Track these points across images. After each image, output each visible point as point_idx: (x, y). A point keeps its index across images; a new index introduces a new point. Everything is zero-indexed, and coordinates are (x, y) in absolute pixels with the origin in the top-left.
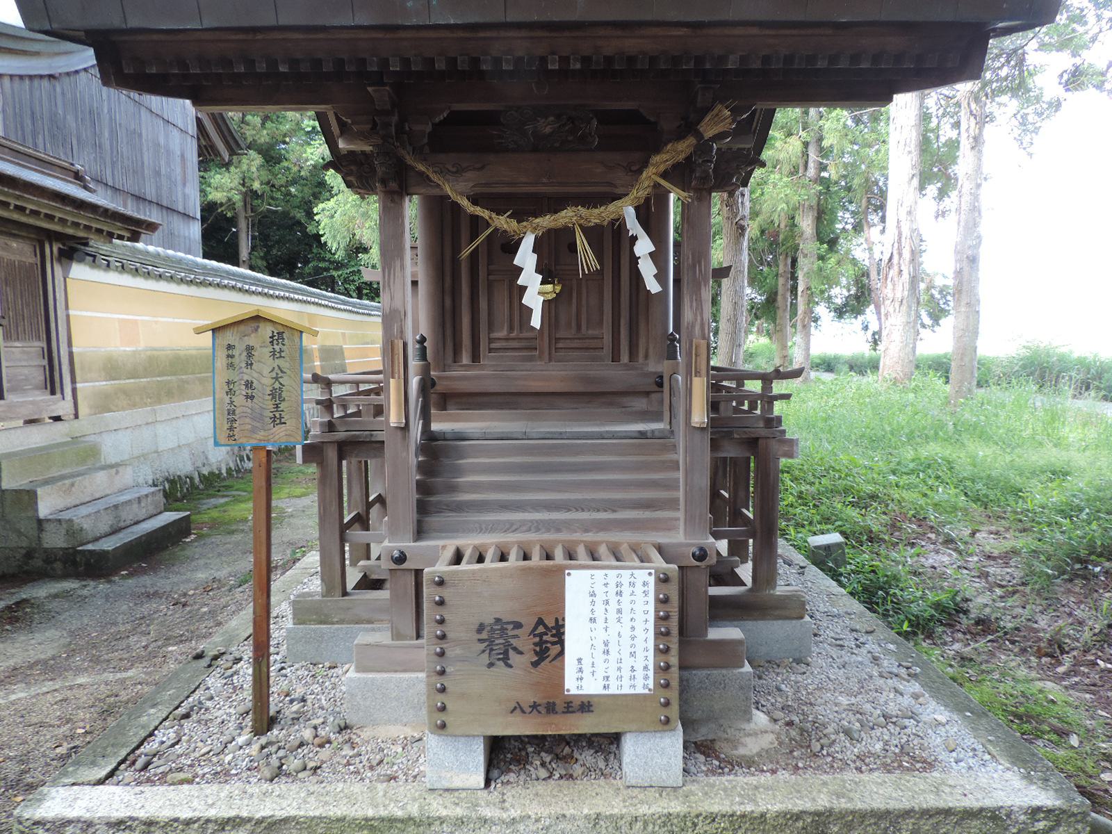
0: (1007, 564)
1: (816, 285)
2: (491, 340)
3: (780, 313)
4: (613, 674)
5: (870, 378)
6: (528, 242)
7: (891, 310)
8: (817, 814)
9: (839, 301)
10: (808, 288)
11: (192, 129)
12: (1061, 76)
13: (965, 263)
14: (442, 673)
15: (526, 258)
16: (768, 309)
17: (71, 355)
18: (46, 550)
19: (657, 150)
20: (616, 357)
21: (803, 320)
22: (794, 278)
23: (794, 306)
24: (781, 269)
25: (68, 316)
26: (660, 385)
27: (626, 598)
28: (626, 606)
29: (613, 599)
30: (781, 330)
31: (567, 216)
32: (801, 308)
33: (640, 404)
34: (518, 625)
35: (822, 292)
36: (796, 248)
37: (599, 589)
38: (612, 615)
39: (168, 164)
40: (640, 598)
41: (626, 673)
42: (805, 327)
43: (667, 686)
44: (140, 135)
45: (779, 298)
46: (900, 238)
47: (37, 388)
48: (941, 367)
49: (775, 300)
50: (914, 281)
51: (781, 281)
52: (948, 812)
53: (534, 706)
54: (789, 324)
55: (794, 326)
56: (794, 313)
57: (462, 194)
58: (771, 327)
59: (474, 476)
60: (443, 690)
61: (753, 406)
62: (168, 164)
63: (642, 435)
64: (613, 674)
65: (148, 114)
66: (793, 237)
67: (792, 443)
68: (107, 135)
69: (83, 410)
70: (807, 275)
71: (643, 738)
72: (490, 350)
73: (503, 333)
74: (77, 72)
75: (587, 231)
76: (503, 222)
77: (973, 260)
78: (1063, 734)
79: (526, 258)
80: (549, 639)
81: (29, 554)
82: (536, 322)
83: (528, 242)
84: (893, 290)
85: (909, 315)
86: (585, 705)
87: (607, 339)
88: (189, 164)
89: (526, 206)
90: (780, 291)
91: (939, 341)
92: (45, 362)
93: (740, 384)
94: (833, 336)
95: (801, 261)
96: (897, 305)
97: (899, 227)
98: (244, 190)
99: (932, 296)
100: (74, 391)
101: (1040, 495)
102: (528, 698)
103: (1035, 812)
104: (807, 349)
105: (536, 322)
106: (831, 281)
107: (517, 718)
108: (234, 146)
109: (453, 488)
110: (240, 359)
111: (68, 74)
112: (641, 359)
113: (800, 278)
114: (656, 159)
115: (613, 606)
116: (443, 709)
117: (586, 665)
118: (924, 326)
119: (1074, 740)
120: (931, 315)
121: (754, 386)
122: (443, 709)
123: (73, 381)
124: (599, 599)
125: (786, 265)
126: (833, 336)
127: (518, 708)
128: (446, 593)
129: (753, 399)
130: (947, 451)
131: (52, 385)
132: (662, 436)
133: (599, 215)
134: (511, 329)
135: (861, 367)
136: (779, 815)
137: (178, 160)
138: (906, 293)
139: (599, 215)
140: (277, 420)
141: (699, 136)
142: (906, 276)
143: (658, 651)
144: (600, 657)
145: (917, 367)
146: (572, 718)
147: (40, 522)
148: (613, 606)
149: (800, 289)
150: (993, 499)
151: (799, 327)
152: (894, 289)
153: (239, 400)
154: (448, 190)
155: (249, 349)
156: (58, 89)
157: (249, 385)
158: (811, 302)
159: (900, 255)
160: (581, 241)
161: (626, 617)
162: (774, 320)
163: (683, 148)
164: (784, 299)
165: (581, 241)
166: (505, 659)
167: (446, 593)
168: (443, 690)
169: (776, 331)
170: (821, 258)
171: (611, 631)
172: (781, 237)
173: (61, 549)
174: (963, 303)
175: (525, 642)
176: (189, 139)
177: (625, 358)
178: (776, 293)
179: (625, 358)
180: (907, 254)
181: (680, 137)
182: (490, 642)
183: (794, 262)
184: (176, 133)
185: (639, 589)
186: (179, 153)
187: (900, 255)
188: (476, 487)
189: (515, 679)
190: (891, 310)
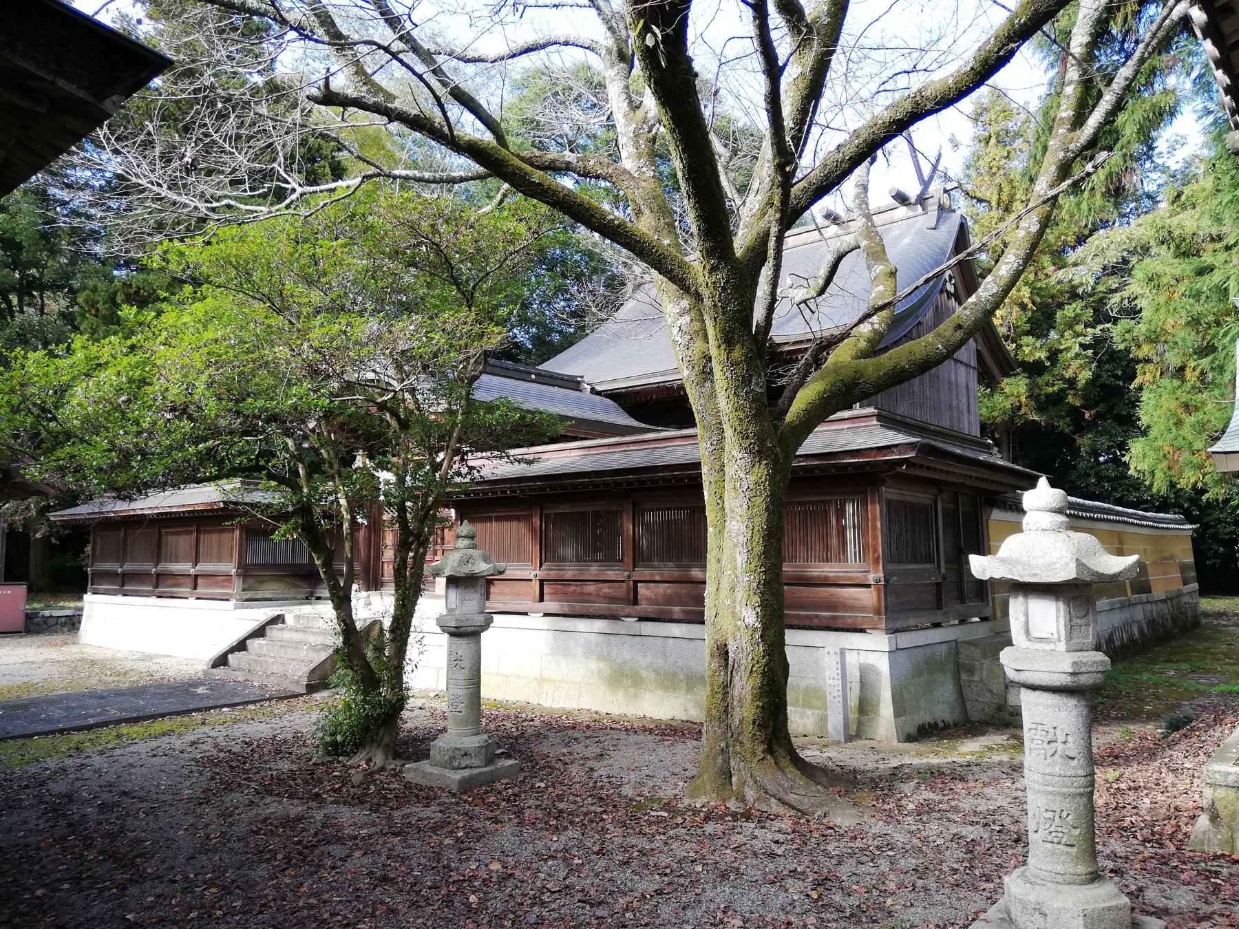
184: (962, 369)
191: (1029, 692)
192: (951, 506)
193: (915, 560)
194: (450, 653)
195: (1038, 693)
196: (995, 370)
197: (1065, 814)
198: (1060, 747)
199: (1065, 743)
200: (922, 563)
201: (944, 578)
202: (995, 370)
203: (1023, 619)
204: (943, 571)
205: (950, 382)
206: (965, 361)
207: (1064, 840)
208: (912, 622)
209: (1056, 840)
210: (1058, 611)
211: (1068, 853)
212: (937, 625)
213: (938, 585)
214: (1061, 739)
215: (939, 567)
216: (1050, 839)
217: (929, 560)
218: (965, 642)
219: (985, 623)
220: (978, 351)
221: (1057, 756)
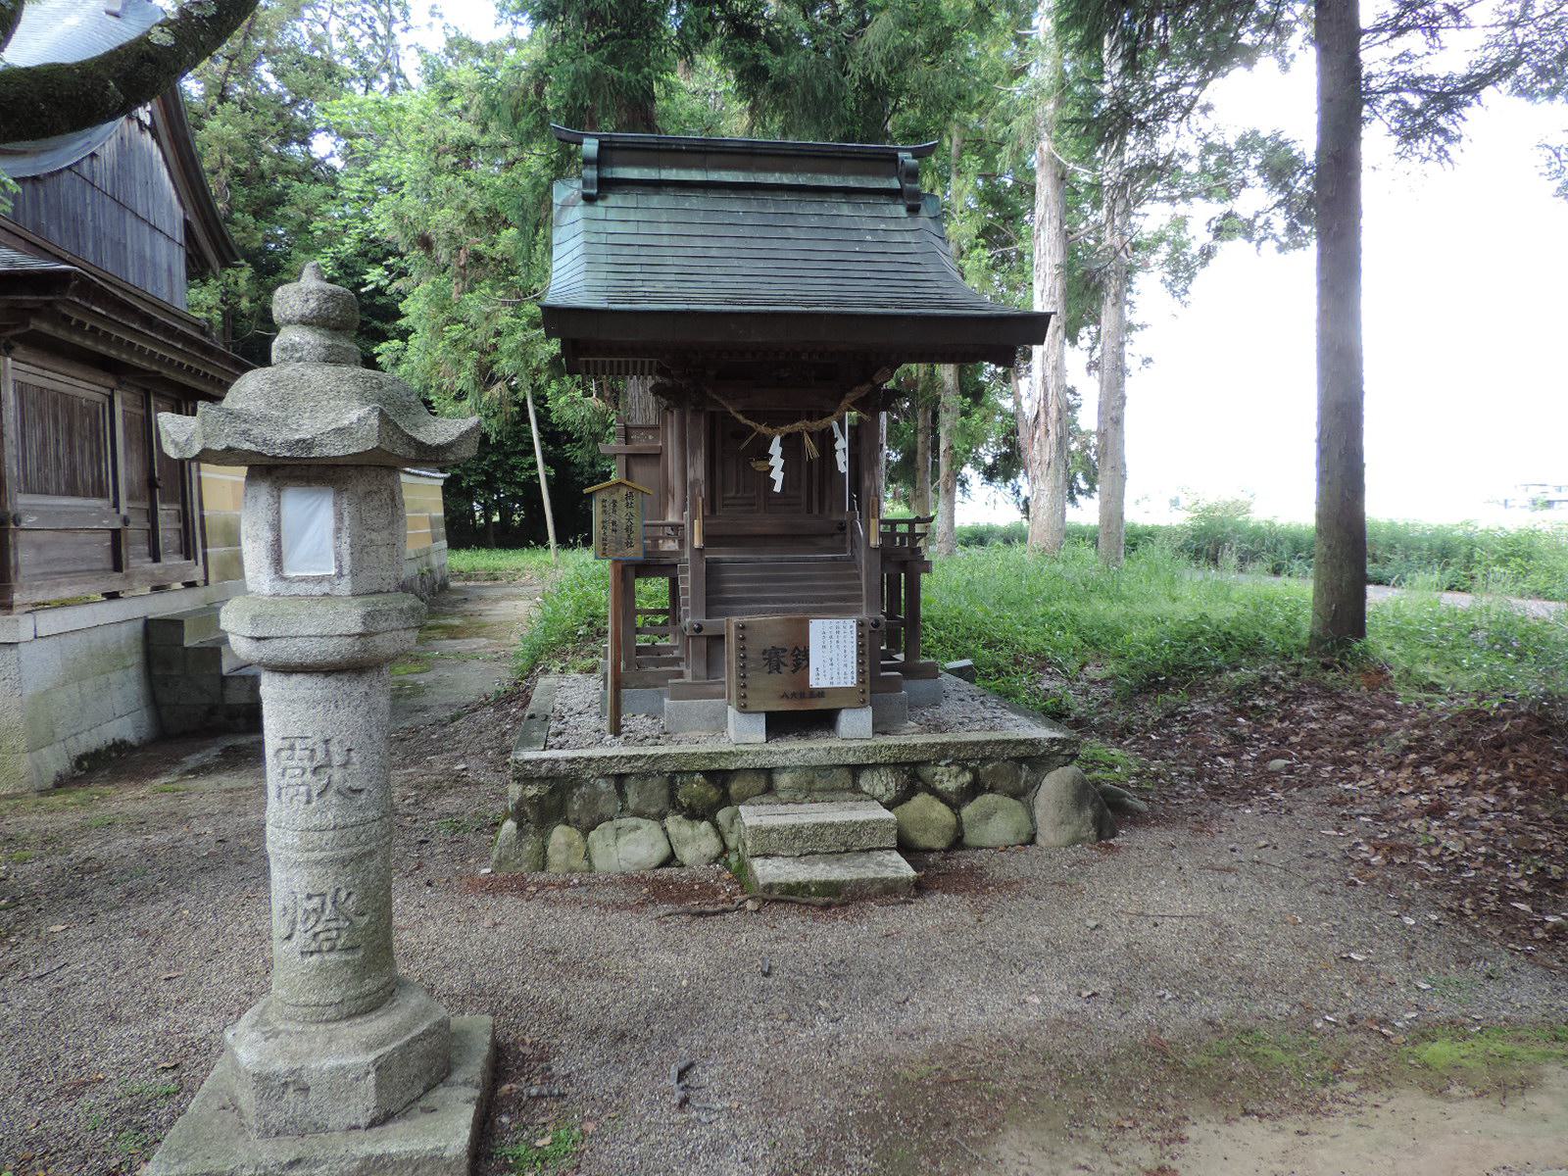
0: (1104, 686)
1: (960, 445)
2: (724, 499)
3: (920, 475)
4: (835, 676)
5: (1018, 548)
6: (777, 440)
7: (1039, 473)
8: (944, 744)
9: (989, 460)
10: (951, 448)
11: (179, 236)
12: (1209, 223)
13: (1109, 425)
14: (744, 677)
15: (776, 449)
16: (907, 471)
17: (202, 517)
18: (229, 706)
19: (850, 390)
20: (810, 511)
21: (946, 484)
22: (934, 430)
23: (936, 466)
24: (920, 424)
25: (199, 478)
26: (844, 528)
27: (842, 634)
28: (841, 639)
29: (834, 635)
30: (922, 496)
31: (799, 426)
32: (944, 470)
33: (827, 542)
34: (785, 650)
35: (968, 451)
36: (937, 400)
37: (827, 630)
38: (834, 644)
39: (155, 282)
40: (849, 636)
41: (842, 676)
42: (950, 492)
43: (863, 682)
44: (125, 247)
45: (919, 458)
46: (1046, 395)
47: (175, 553)
48: (1091, 537)
49: (914, 460)
50: (1061, 442)
51: (921, 438)
52: (1009, 741)
53: (794, 694)
54: (930, 489)
55: (936, 491)
56: (936, 476)
57: (741, 412)
58: (910, 492)
59: (733, 585)
60: (745, 686)
61: (902, 542)
62: (155, 282)
63: (834, 559)
64: (835, 676)
65: (134, 219)
66: (934, 388)
67: (929, 563)
68: (90, 246)
69: (212, 578)
70: (950, 432)
71: (851, 712)
72: (724, 505)
73: (732, 494)
74: (60, 171)
75: (811, 435)
76: (762, 429)
77: (1117, 422)
78: (1112, 767)
79: (776, 449)
80: (800, 657)
81: (212, 710)
82: (777, 488)
83: (777, 440)
84: (1039, 450)
85: (1057, 479)
86: (821, 693)
87: (804, 498)
88: (176, 281)
89: (775, 420)
90: (920, 451)
91: (1086, 513)
92: (180, 526)
93: (893, 528)
94: (981, 504)
95: (943, 416)
96: (1045, 466)
97: (1044, 383)
98: (225, 308)
99: (1088, 458)
100: (205, 555)
101: (1136, 634)
102: (790, 690)
103: (1052, 741)
104: (952, 517)
105: (777, 488)
106: (975, 439)
107: (784, 701)
108: (227, 254)
109: (721, 591)
110: (609, 508)
111: (51, 174)
112: (827, 512)
113: (942, 435)
114: (849, 395)
115: (835, 639)
116: (745, 697)
117: (821, 671)
118: (1080, 492)
119: (1118, 770)
120: (1086, 478)
121: (903, 528)
122: (745, 697)
123: (204, 546)
124: (828, 635)
125: (925, 419)
126: (981, 504)
127: (785, 696)
128: (746, 633)
129: (903, 536)
130: (1073, 607)
131: (187, 550)
132: (848, 560)
133: (817, 425)
134: (737, 492)
135: (1011, 537)
136: (923, 745)
137: (165, 275)
138: (1053, 455)
139: (817, 425)
140: (629, 544)
141: (873, 382)
142: (1052, 437)
143: (858, 663)
144: (828, 667)
145: (1067, 535)
146: (813, 700)
147: (224, 679)
148: (835, 639)
149: (942, 447)
150: (1097, 641)
151: (942, 492)
152: (1041, 450)
153: (609, 532)
154: (731, 410)
155: (615, 502)
156: (42, 194)
157: (614, 523)
158: (957, 462)
159: (1047, 413)
160: (807, 439)
161: (841, 645)
162: (913, 483)
163: (865, 389)
164: (924, 459)
165: (807, 439)
166: (778, 669)
167: (746, 633)
168: (745, 686)
169: (917, 497)
170: (965, 413)
171: (833, 653)
172: (920, 387)
173: (245, 705)
174: (1108, 467)
175: (788, 660)
176: (176, 246)
177: (816, 511)
178: (915, 452)
179: (816, 511)
180: (1053, 414)
181: (862, 383)
182: (770, 660)
183: (935, 416)
184: (162, 241)
185: (848, 630)
186: (165, 266)
187: (1047, 413)
188: (735, 590)
189: (779, 681)
190: (1039, 473)
191: (277, 678)
192: (141, 412)
193: (72, 491)
194: (1159, 528)
195: (296, 679)
196: (211, 256)
197: (343, 894)
198: (337, 775)
199: (344, 765)
200: (86, 496)
201: (126, 521)
202: (211, 256)
203: (268, 535)
204: (123, 511)
205: (142, 257)
206: (167, 231)
207: (339, 943)
208: (66, 593)
209: (326, 946)
210: (339, 517)
211: (347, 963)
212: (112, 596)
213: (116, 534)
214: (337, 759)
215: (116, 505)
216: (314, 946)
217: (99, 491)
218: (545, 848)
219: (191, 591)
220: (186, 221)
221: (331, 792)
